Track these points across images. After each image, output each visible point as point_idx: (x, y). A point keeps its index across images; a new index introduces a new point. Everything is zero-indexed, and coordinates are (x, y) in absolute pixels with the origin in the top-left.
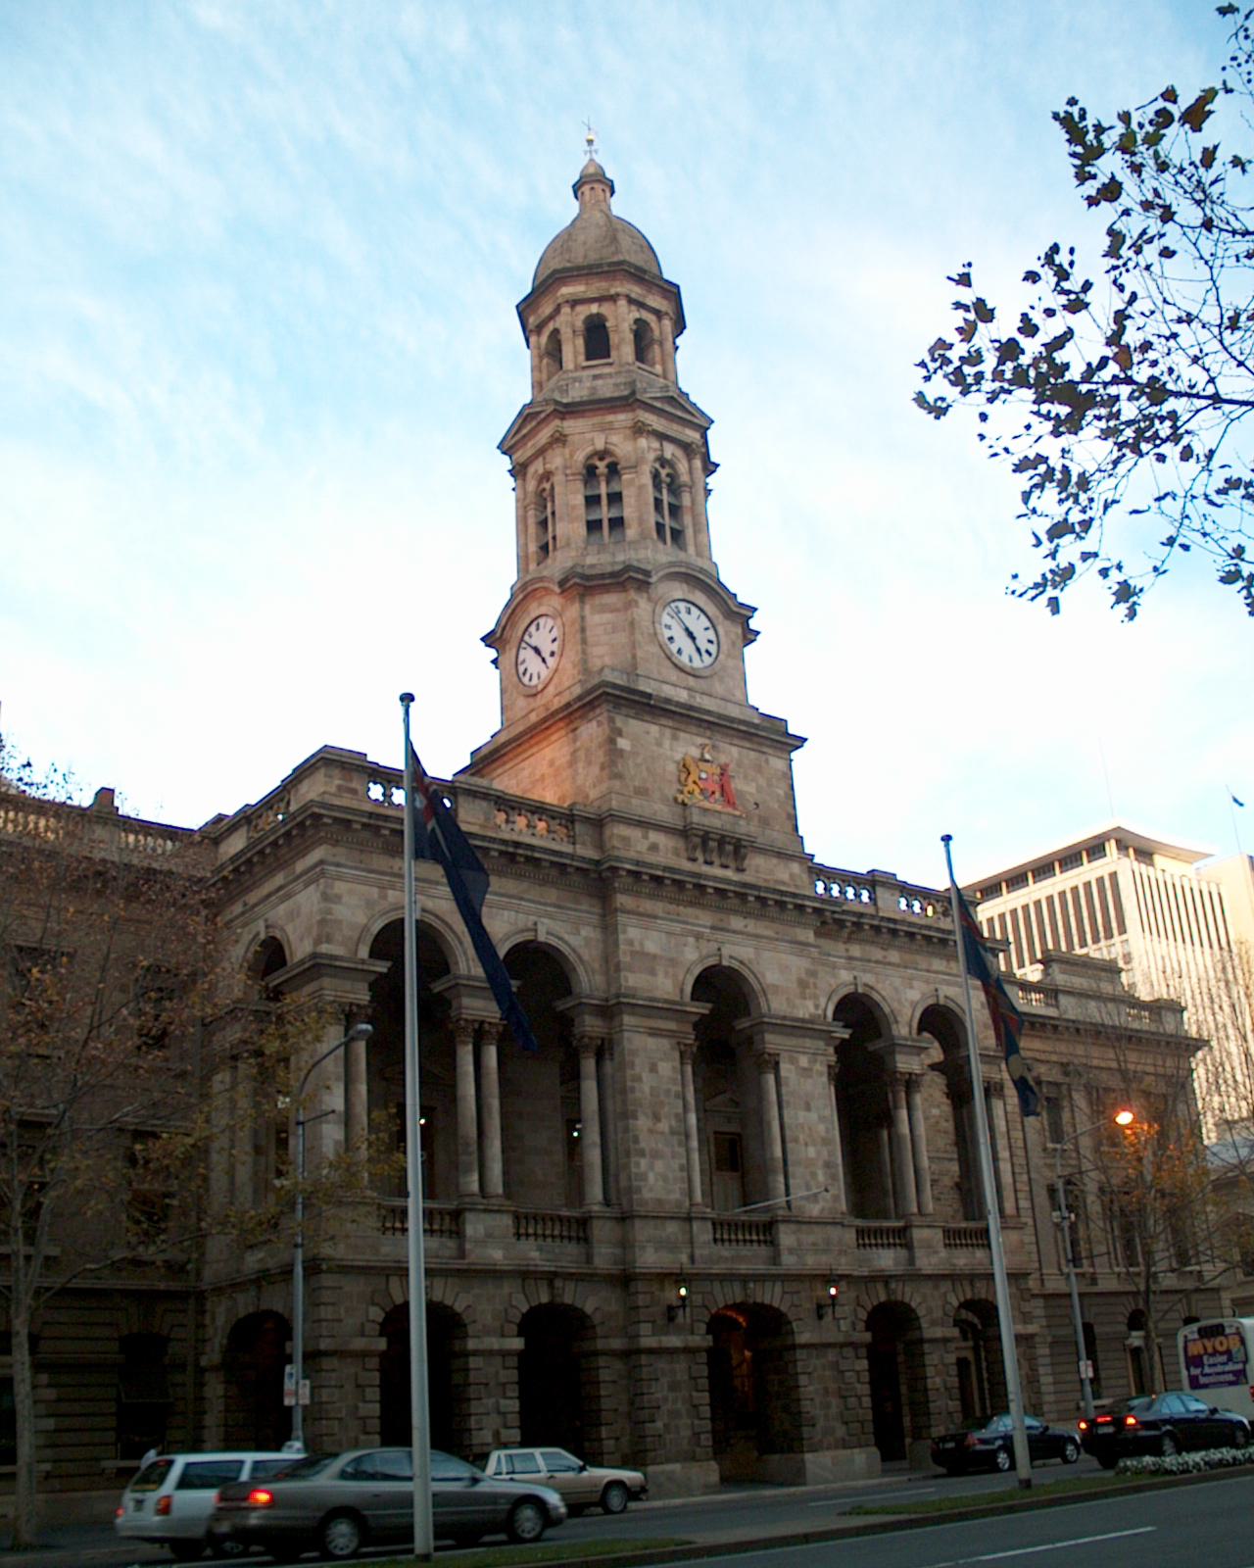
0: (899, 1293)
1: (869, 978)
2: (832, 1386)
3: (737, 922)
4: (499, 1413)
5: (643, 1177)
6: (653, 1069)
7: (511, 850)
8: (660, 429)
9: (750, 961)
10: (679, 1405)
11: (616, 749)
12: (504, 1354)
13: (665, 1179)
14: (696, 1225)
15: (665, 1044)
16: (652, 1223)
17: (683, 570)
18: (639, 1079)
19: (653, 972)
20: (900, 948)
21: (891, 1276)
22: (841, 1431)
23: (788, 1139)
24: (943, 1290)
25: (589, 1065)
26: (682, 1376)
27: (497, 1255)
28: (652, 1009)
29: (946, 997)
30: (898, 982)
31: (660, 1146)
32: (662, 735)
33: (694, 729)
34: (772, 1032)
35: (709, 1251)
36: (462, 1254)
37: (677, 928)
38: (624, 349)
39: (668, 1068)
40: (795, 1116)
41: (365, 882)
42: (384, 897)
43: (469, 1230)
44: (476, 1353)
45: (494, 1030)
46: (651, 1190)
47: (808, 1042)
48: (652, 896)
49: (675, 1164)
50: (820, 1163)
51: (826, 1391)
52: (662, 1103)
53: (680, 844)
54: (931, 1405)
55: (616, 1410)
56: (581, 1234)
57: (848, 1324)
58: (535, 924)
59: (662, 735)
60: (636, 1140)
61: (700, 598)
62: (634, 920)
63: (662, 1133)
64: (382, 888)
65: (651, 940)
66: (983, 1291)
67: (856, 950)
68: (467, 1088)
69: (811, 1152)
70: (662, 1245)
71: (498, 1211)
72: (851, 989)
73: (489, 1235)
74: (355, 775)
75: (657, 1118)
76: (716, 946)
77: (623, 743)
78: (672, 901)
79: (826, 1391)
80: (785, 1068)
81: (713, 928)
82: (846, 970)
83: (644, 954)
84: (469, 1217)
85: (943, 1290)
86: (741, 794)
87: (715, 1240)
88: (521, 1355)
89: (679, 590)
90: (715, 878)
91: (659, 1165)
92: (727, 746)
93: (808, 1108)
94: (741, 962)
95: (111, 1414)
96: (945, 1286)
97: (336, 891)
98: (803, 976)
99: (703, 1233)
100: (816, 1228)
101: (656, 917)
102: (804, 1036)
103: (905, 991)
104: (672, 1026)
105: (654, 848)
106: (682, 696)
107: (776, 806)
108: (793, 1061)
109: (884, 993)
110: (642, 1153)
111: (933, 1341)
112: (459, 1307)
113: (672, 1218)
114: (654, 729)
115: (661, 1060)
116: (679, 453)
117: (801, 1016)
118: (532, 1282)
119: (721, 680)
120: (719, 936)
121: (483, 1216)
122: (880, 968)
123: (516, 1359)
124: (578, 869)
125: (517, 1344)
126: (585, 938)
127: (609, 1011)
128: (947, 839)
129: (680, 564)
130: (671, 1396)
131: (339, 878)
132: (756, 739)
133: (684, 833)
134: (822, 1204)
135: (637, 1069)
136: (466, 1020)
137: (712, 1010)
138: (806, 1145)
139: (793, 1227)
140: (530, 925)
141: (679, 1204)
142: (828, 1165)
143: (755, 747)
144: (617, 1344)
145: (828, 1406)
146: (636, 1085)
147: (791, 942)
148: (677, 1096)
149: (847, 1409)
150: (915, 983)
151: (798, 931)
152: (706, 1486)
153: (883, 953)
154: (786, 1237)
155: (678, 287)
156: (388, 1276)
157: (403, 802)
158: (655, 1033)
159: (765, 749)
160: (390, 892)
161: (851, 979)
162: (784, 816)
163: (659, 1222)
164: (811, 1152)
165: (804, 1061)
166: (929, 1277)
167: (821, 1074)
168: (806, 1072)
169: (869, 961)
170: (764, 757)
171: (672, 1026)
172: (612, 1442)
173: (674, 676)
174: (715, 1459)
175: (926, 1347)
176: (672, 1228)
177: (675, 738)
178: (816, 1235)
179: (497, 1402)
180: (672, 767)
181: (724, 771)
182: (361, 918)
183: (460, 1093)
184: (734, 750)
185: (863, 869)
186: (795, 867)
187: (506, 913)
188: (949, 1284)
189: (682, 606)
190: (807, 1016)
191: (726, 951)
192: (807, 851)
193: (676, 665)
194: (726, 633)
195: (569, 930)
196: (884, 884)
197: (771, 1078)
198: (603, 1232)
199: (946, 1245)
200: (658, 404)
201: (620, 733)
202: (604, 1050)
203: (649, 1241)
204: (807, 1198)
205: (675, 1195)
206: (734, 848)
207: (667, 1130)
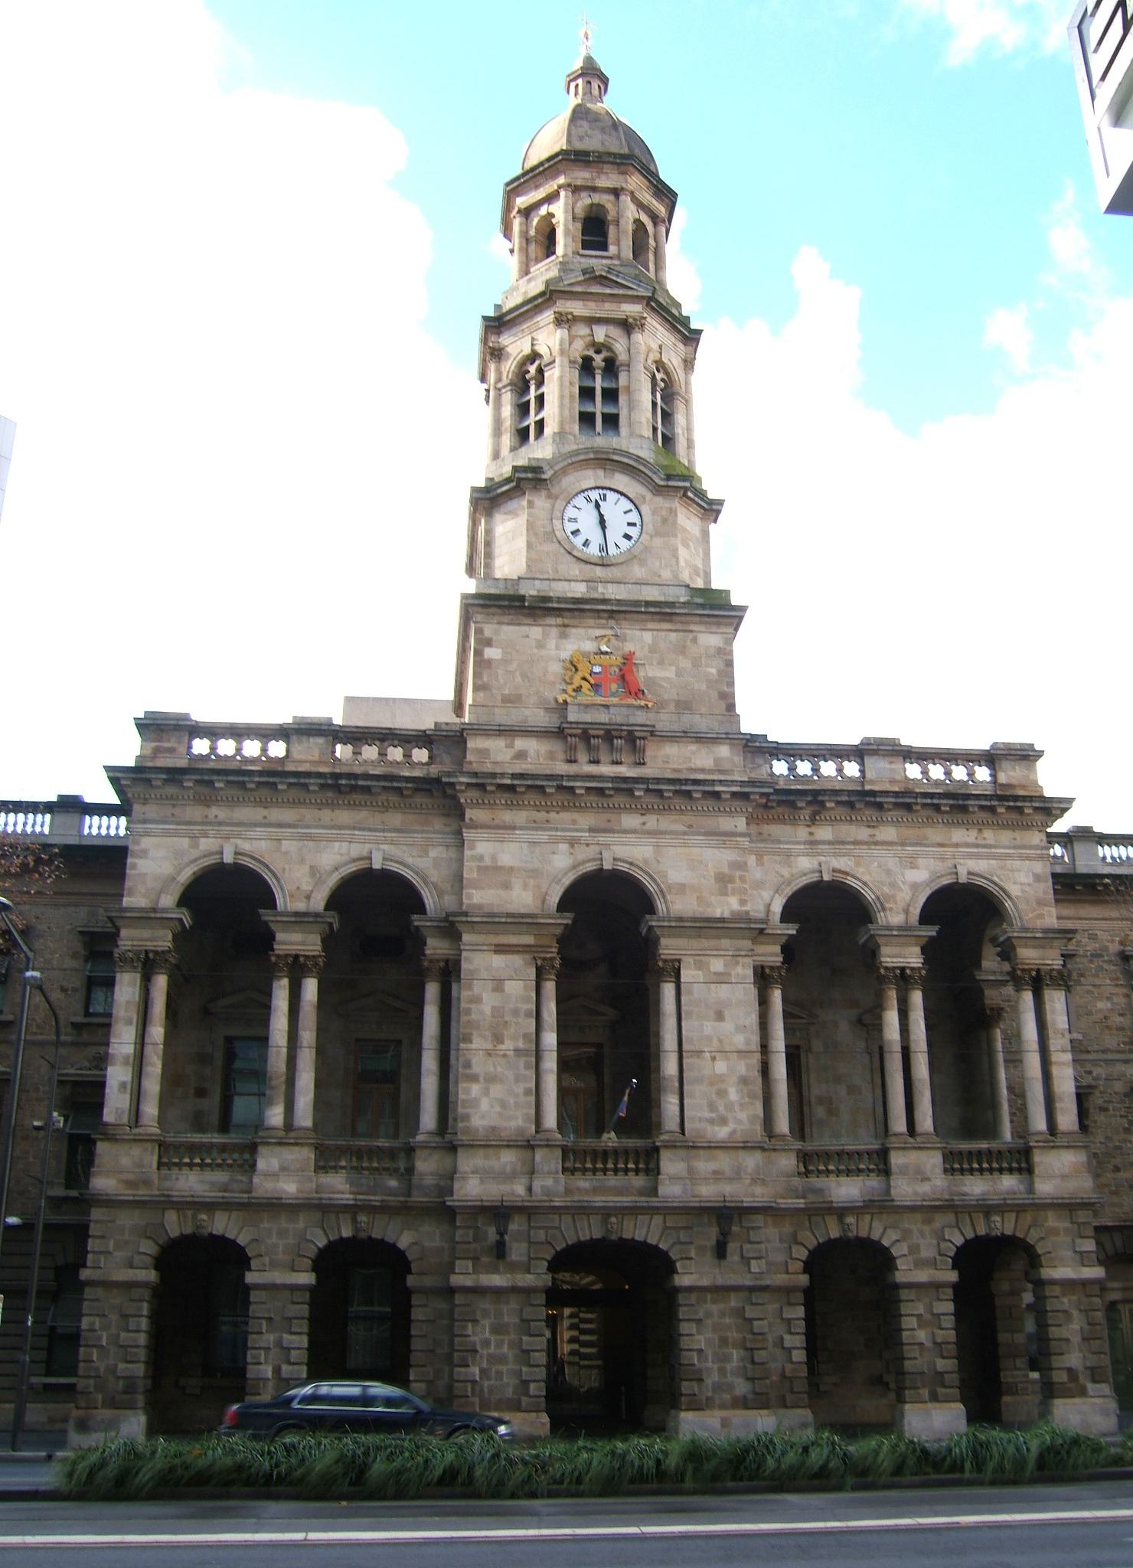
0: (854, 1228)
1: (842, 863)
2: (734, 1335)
3: (630, 820)
4: (283, 1348)
5: (474, 1103)
8: (586, 313)
9: (645, 861)
10: (505, 1349)
12: (294, 1288)
13: (503, 1105)
14: (539, 1155)
16: (481, 1152)
18: (478, 1000)
19: (507, 886)
20: (896, 823)
22: (742, 1387)
24: (937, 1225)
25: (432, 990)
26: (510, 1319)
27: (289, 1188)
28: (502, 923)
30: (892, 864)
31: (499, 1069)
33: (591, 622)
34: (1026, 946)
35: (550, 1181)
38: (621, 245)
39: (519, 988)
41: (175, 834)
42: (196, 846)
43: (261, 1164)
44: (258, 1287)
45: (916, 976)
46: (483, 1117)
48: (510, 806)
49: (520, 1089)
50: (734, 1079)
53: (557, 747)
54: (907, 1363)
55: (433, 1351)
56: (881, 1166)
57: (776, 1259)
59: (545, 635)
61: (621, 481)
62: (485, 834)
64: (193, 837)
65: (510, 853)
66: (999, 1225)
67: (824, 833)
68: (279, 1023)
69: (721, 1067)
70: (485, 1175)
71: (296, 1144)
72: (815, 877)
75: (498, 1039)
76: (597, 848)
78: (537, 808)
79: (724, 1342)
80: (686, 975)
81: (591, 830)
82: (804, 857)
83: (497, 869)
85: (937, 1225)
86: (652, 682)
87: (564, 1170)
88: (312, 1290)
89: (590, 477)
91: (497, 1090)
92: (638, 633)
93: (720, 1016)
94: (631, 864)
96: (940, 1220)
97: (143, 846)
98: (726, 870)
99: (548, 1161)
100: (720, 1154)
101: (514, 828)
102: (719, 937)
103: (897, 875)
104: (528, 940)
105: (521, 755)
106: (579, 590)
107: (704, 687)
108: (700, 966)
109: (866, 878)
110: (474, 1078)
111: (910, 1286)
112: (242, 1240)
113: (508, 1146)
114: (536, 632)
116: (616, 332)
118: (333, 1216)
120: (603, 838)
121: (278, 1149)
122: (863, 851)
123: (308, 1294)
124: (734, 794)
125: (307, 1278)
127: (450, 928)
131: (147, 834)
133: (559, 733)
134: (731, 1126)
136: (887, 968)
137: (575, 921)
138: (714, 1059)
139: (683, 1153)
140: (365, 854)
141: (520, 1131)
143: (679, 627)
144: (428, 1281)
145: (725, 1359)
146: (473, 1006)
148: (528, 1015)
149: (753, 1362)
154: (671, 1165)
156: (355, 1213)
158: (501, 949)
159: (692, 627)
160: (202, 840)
161: (816, 866)
162: (715, 695)
163: (491, 1151)
164: (721, 1067)
166: (913, 1209)
168: (721, 979)
169: (843, 843)
170: (691, 636)
173: (576, 570)
174: (810, 1407)
175: (904, 1294)
177: (563, 636)
178: (723, 1162)
179: (281, 1338)
180: (556, 668)
181: (628, 658)
182: (166, 868)
184: (648, 637)
185: (855, 740)
186: (724, 751)
187: (337, 844)
188: (950, 1218)
190: (727, 915)
191: (607, 855)
194: (654, 512)
195: (408, 850)
196: (875, 752)
197: (668, 990)
199: (946, 1171)
200: (579, 289)
201: (489, 643)
202: (450, 972)
204: (711, 1121)
205: (519, 1121)
206: (631, 740)
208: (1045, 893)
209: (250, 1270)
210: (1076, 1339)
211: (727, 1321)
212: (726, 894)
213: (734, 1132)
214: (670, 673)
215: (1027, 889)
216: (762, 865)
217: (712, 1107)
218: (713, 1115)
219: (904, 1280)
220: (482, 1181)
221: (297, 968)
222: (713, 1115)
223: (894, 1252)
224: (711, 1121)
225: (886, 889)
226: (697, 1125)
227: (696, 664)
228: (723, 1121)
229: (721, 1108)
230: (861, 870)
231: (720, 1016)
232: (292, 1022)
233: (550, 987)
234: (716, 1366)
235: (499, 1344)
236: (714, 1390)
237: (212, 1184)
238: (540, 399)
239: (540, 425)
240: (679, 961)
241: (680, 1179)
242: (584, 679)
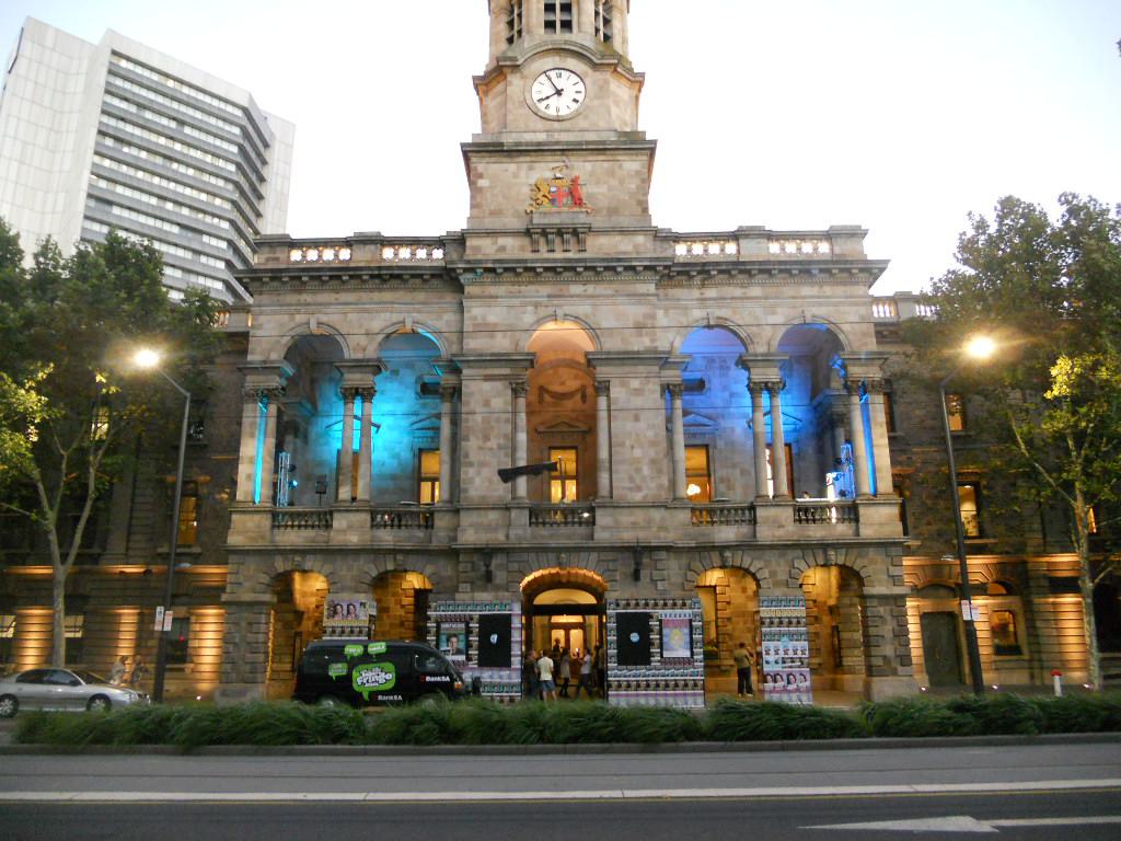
5: (471, 481)
7: (376, 272)
9: (586, 316)
11: (476, 188)
15: (498, 385)
17: (550, 47)
21: (828, 545)
23: (613, 444)
29: (814, 316)
31: (487, 458)
32: (519, 169)
36: (592, 537)
37: (516, 302)
40: (623, 426)
42: (293, 319)
46: (476, 490)
47: (641, 369)
52: (492, 427)
53: (526, 241)
56: (852, 516)
58: (803, 312)
60: (467, 456)
61: (572, 63)
63: (491, 449)
69: (637, 453)
73: (350, 527)
74: (278, 249)
75: (487, 438)
77: (482, 183)
81: (549, 296)
84: (336, 515)
90: (561, 260)
92: (581, 164)
95: (181, 628)
104: (506, 371)
105: (503, 249)
106: (542, 137)
107: (627, 198)
108: (623, 385)
113: (493, 509)
115: (495, 397)
117: (636, 349)
118: (810, 551)
119: (586, 117)
121: (345, 515)
126: (447, 321)
129: (553, 42)
132: (608, 152)
138: (632, 447)
142: (653, 462)
143: (610, 158)
147: (628, 295)
150: (779, 310)
151: (638, 286)
153: (744, 290)
157: (418, 257)
158: (488, 378)
162: (634, 203)
165: (635, 384)
166: (772, 547)
167: (653, 392)
171: (506, 371)
173: (540, 125)
176: (493, 516)
180: (526, 190)
181: (575, 181)
184: (588, 166)
186: (640, 239)
189: (553, 74)
192: (654, 224)
193: (541, 117)
196: (747, 236)
198: (442, 522)
203: (471, 526)
204: (631, 489)
207: (495, 446)
214: (603, 189)
217: (631, 479)
222: (632, 485)
224: (631, 489)
228: (639, 489)
230: (737, 317)
237: (305, 538)
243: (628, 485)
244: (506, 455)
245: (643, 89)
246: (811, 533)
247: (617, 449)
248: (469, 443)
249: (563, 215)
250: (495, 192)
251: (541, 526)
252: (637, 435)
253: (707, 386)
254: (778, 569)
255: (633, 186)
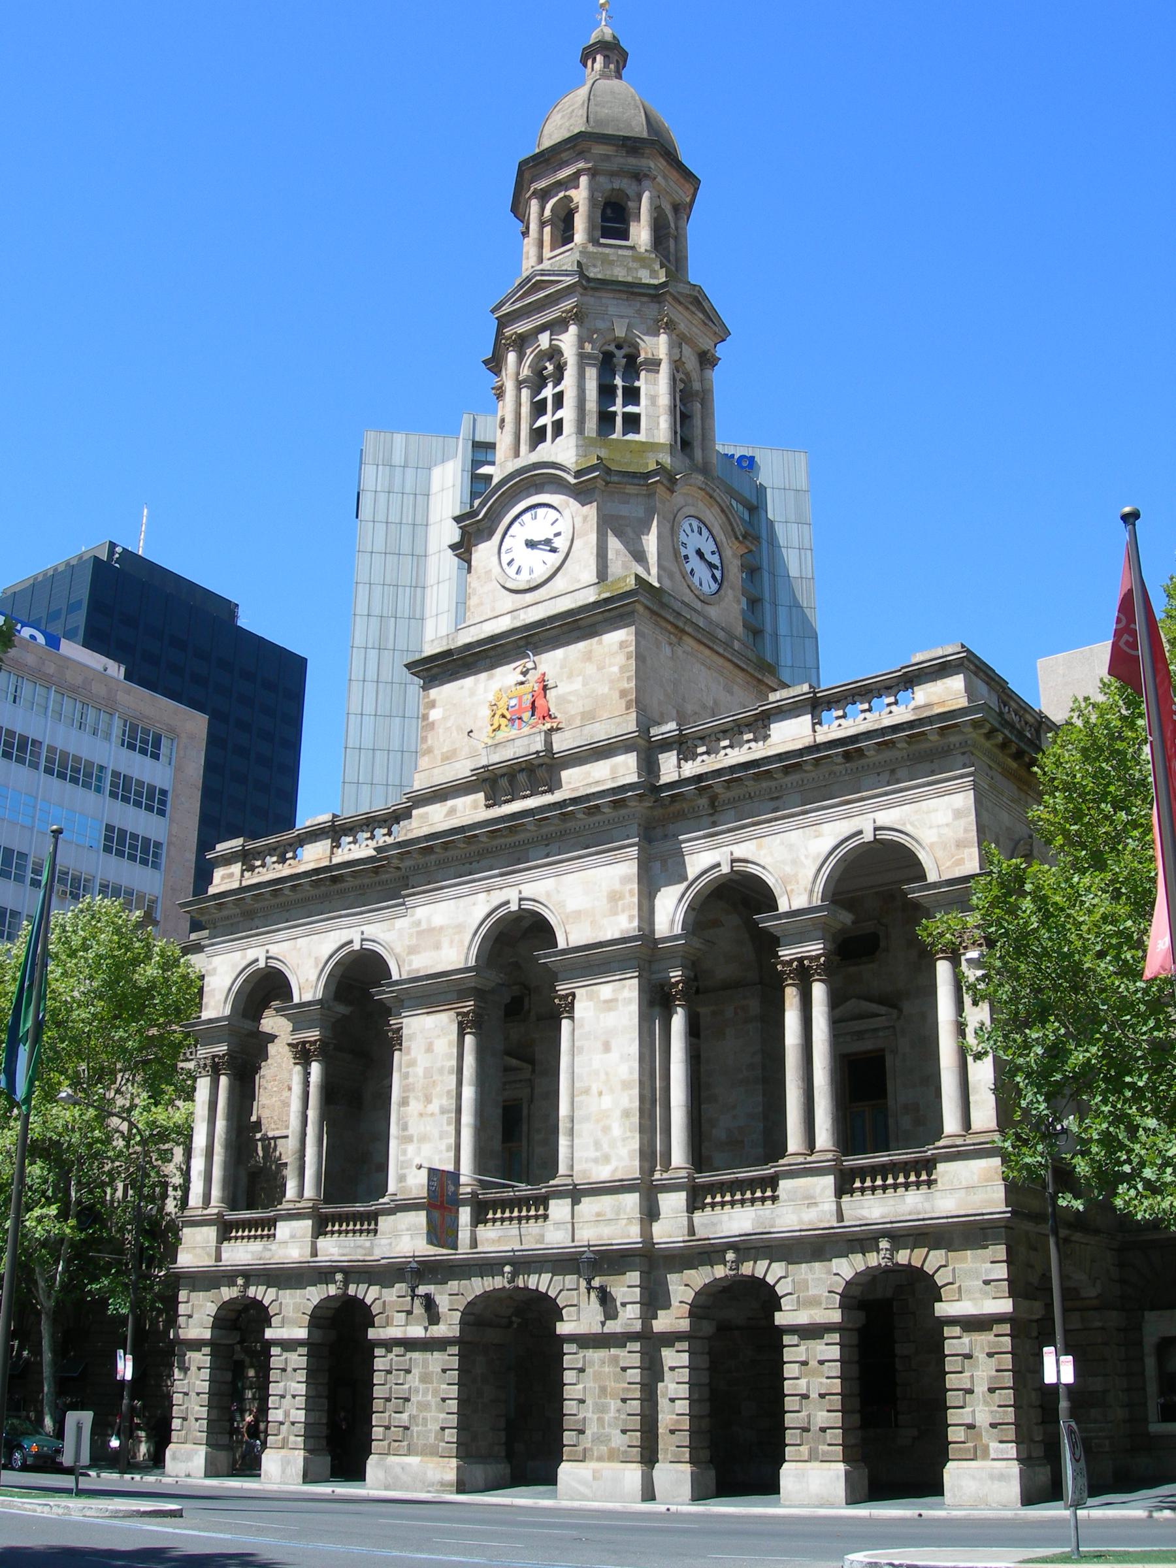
6: (429, 1049)
31: (428, 1128)
50: (617, 1113)
51: (603, 1390)
63: (432, 1114)
73: (293, 1236)
75: (428, 1100)
79: (603, 1390)
83: (431, 930)
128: (1130, 518)
130: (422, 1386)
134: (614, 1163)
135: (413, 1054)
138: (600, 1094)
146: (410, 1070)
152: (442, 1484)
155: (521, 164)
164: (607, 1102)
167: (628, 1001)
172: (179, 1421)
183: (317, 1112)
197: (565, 1024)
204: (596, 1161)
207: (437, 1110)
208: (966, 831)
209: (270, 1326)
210: (981, 1388)
211: (607, 1369)
212: (616, 914)
213: (616, 1170)
214: (577, 685)
215: (945, 830)
216: (667, 870)
217: (597, 1145)
218: (598, 1154)
219: (784, 1323)
220: (412, 1238)
221: (804, 975)
222: (598, 1154)
223: (780, 1290)
224: (596, 1161)
225: (788, 869)
226: (584, 1166)
227: (600, 668)
228: (606, 1159)
229: (605, 1147)
230: (762, 852)
231: (607, 1047)
232: (808, 1029)
233: (469, 1040)
234: (595, 1417)
235: (425, 1393)
236: (593, 1441)
237: (252, 1253)
238: (559, 399)
239: (558, 426)
240: (574, 995)
241: (558, 1228)
242: (503, 716)
243: (593, 1154)
244: (449, 1124)
245: (473, 563)
246: (865, 1213)
247: (583, 1097)
248: (409, 1109)
249: (523, 743)
250: (449, 725)
251: (901, 1190)
252: (607, 1074)
253: (882, 944)
254: (810, 1277)
255: (615, 669)
